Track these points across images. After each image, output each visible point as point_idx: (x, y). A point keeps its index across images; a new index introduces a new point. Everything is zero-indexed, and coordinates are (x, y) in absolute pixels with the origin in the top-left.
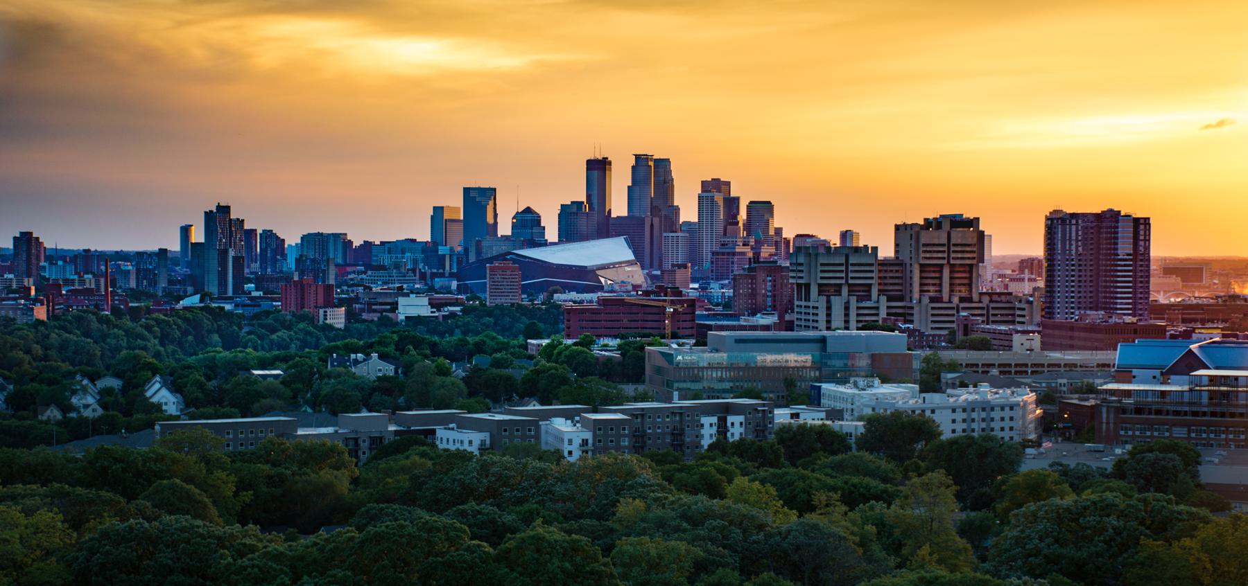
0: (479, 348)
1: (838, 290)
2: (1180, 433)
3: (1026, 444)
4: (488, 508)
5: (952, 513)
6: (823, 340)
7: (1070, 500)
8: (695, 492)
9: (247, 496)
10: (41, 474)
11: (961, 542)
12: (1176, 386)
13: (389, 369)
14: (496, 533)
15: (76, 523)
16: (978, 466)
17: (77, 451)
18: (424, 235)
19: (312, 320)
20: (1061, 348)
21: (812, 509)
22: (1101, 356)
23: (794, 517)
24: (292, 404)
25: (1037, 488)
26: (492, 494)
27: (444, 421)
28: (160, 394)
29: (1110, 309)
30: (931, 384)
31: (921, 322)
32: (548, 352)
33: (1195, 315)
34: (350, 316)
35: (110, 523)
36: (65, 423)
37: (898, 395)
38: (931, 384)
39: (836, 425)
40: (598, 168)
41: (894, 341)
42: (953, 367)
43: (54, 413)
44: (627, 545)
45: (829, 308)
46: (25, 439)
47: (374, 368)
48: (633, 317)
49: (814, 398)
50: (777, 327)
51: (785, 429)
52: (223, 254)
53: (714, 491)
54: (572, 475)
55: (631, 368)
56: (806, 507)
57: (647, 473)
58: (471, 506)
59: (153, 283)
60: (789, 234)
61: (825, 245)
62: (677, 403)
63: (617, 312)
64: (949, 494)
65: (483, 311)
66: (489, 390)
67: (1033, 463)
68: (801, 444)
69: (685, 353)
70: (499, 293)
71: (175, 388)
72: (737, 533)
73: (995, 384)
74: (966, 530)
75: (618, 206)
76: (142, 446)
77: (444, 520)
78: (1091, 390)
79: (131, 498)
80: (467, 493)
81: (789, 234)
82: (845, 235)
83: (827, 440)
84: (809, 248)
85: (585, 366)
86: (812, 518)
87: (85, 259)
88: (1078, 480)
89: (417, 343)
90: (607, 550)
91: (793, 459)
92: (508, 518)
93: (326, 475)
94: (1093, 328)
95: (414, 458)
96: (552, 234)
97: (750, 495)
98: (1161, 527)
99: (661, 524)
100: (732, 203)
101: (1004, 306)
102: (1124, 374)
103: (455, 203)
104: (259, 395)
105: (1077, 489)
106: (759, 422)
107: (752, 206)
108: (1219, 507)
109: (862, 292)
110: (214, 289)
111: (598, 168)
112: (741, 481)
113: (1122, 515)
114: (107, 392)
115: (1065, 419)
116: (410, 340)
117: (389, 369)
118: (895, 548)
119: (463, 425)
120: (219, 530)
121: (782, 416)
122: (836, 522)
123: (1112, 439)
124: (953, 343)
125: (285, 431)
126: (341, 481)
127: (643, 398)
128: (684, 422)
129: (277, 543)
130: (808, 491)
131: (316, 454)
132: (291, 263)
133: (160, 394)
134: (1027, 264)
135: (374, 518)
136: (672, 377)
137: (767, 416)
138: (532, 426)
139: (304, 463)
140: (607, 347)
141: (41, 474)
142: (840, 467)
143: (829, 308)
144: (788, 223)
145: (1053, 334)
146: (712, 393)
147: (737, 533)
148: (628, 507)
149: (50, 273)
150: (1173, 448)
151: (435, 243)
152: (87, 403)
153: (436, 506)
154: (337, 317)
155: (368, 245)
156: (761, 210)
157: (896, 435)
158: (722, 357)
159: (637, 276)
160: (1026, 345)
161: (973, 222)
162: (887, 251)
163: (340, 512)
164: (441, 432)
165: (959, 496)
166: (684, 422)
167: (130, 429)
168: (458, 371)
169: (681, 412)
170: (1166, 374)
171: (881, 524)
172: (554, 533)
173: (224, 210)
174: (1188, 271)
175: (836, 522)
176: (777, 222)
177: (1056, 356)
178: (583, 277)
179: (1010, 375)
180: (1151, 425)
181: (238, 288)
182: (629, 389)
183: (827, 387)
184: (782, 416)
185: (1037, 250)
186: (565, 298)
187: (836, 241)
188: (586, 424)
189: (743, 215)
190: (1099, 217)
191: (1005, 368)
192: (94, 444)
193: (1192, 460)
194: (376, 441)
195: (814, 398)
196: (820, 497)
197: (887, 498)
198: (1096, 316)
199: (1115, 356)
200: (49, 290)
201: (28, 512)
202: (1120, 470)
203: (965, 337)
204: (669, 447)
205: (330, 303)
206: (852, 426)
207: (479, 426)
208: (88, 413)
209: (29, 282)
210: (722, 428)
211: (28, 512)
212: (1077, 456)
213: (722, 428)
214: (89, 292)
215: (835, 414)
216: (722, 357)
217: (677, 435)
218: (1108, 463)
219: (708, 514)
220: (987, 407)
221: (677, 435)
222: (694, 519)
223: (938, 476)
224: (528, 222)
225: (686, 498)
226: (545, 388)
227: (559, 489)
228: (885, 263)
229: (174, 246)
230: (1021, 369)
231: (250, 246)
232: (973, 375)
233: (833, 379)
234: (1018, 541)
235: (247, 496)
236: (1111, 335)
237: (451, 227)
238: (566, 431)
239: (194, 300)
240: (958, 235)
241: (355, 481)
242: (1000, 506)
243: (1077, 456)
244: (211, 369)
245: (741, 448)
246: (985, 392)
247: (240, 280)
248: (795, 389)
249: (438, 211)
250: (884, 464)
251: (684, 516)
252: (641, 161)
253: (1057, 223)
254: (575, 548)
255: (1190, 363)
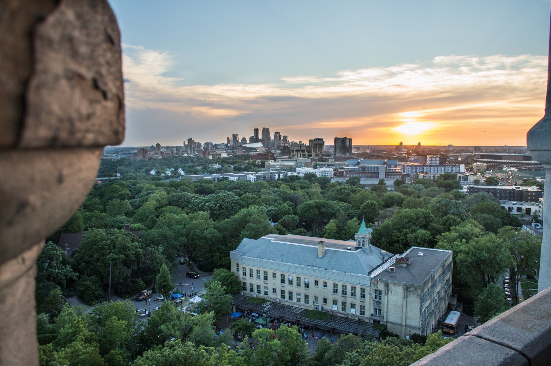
0: (236, 162)
1: (299, 151)
2: (357, 175)
3: (332, 178)
4: (238, 191)
5: (319, 190)
6: (296, 160)
7: (339, 187)
8: (274, 187)
9: (196, 189)
10: (162, 185)
11: (321, 195)
12: (356, 167)
13: (220, 166)
14: (240, 195)
15: (168, 193)
16: (324, 182)
17: (168, 181)
18: (226, 143)
19: (206, 158)
20: (337, 161)
21: (295, 190)
22: (344, 162)
23: (292, 191)
24: (203, 173)
25: (333, 185)
26: (239, 188)
27: (230, 175)
28: (181, 171)
29: (345, 154)
30: (315, 168)
31: (314, 156)
32: (248, 163)
33: (359, 155)
34: (213, 157)
35: (173, 194)
36: (165, 176)
37: (310, 170)
38: (315, 168)
39: (299, 175)
40: (256, 130)
41: (309, 160)
42: (319, 165)
43: (163, 175)
44: (263, 197)
45: (430, 170)
46: (159, 179)
47: (217, 166)
48: (264, 157)
49: (295, 170)
50: (288, 158)
51: (290, 176)
52: (191, 146)
53: (278, 187)
54: (252, 184)
55: (263, 166)
56: (294, 190)
57: (266, 184)
58: (235, 190)
59: (179, 152)
60: (290, 141)
61: (296, 143)
62: (271, 171)
63: (259, 156)
64: (319, 187)
65: (237, 156)
66: (237, 170)
67: (333, 181)
68: (293, 178)
69: (272, 163)
70: (239, 152)
71: (183, 170)
72: (282, 194)
73: (326, 167)
74: (322, 193)
75: (260, 137)
76: (178, 180)
77: (230, 193)
78: (342, 168)
79: (177, 189)
80: (235, 188)
81: (290, 141)
82: (300, 142)
83: (298, 178)
84: (294, 144)
85: (255, 165)
86: (295, 191)
87: (168, 148)
88: (340, 184)
89: (225, 162)
90: (260, 198)
91: (292, 181)
92: (242, 192)
93: (210, 185)
94: (343, 158)
95: (225, 181)
96: (248, 142)
97: (284, 187)
98: (354, 192)
99: (269, 193)
100: (280, 136)
101: (328, 154)
102: (348, 166)
103: (231, 138)
104: (198, 171)
105: (340, 185)
106: (286, 175)
107: (284, 137)
108: (363, 188)
109: (303, 151)
110: (189, 152)
111: (256, 130)
112: (283, 185)
113: (348, 190)
114: (172, 171)
115: (338, 174)
116: (223, 161)
117: (220, 166)
118: (310, 196)
119: (233, 176)
120: (192, 195)
121: (289, 174)
122: (299, 192)
123: (346, 177)
124: (319, 161)
125: (202, 177)
126: (212, 186)
127: (265, 171)
128: (272, 175)
129: (202, 197)
130: (294, 187)
131: (209, 182)
132: (202, 148)
133: (181, 171)
134: (331, 146)
135: (218, 193)
136: (270, 167)
137: (287, 174)
138: (245, 176)
139: (206, 183)
140: (258, 162)
141: (162, 185)
142: (300, 182)
143: (430, 170)
144: (290, 140)
145: (336, 159)
146: (277, 170)
147: (282, 194)
148: (263, 190)
149: (162, 150)
150: (356, 178)
151: (228, 144)
152: (169, 173)
153: (229, 190)
154: (211, 157)
155: (216, 144)
156: (285, 137)
157: (310, 177)
158: (279, 163)
159: (264, 149)
160: (331, 161)
161: (322, 139)
162: (307, 144)
163: (212, 192)
164: (229, 177)
165: (321, 187)
166: (272, 175)
167: (176, 177)
168: (232, 167)
169: (272, 173)
170: (355, 166)
171: (307, 193)
172: (250, 195)
173: (191, 139)
174: (358, 148)
175: (299, 192)
176: (288, 139)
177: (336, 162)
178: (255, 149)
179: (329, 166)
180: (352, 174)
181: (194, 153)
182: (262, 169)
183: (297, 168)
184: (289, 174)
185: (333, 144)
186: (251, 153)
187: (298, 143)
188: (255, 175)
189: (282, 138)
190: (343, 138)
191: (328, 165)
192: (170, 180)
193: (359, 180)
194: (218, 179)
195: (295, 170)
196: (297, 188)
197: (308, 188)
198: (343, 155)
199: (347, 162)
200: (162, 153)
201: (160, 192)
202: (347, 182)
203: (321, 160)
204: (270, 180)
205: (209, 155)
206: (302, 175)
207: (236, 176)
208: (169, 175)
209: (159, 152)
210: (279, 176)
211: (160, 192)
212: (340, 180)
213: (279, 176)
214: (168, 154)
215: (299, 173)
216: (279, 163)
217: (271, 177)
218: (345, 181)
219: (277, 191)
220: (325, 172)
221: (271, 177)
222: (275, 192)
223: (317, 184)
224: (244, 140)
225: (273, 188)
226: (247, 169)
227: (251, 187)
228: (307, 147)
229: (183, 145)
230: (331, 165)
231: (195, 145)
232: (322, 166)
233: (298, 167)
234: (331, 195)
235: (196, 189)
236: (346, 159)
237: (458, 168)
238: (252, 177)
239: (186, 155)
240: (320, 142)
241: (215, 186)
242: (327, 188)
243: (340, 180)
244: (189, 167)
245: (282, 180)
246: (324, 169)
247: (194, 151)
248: (291, 169)
249: (228, 138)
250: (307, 181)
251: (273, 192)
252: (264, 129)
253: (336, 140)
254: (254, 198)
255: (358, 163)
